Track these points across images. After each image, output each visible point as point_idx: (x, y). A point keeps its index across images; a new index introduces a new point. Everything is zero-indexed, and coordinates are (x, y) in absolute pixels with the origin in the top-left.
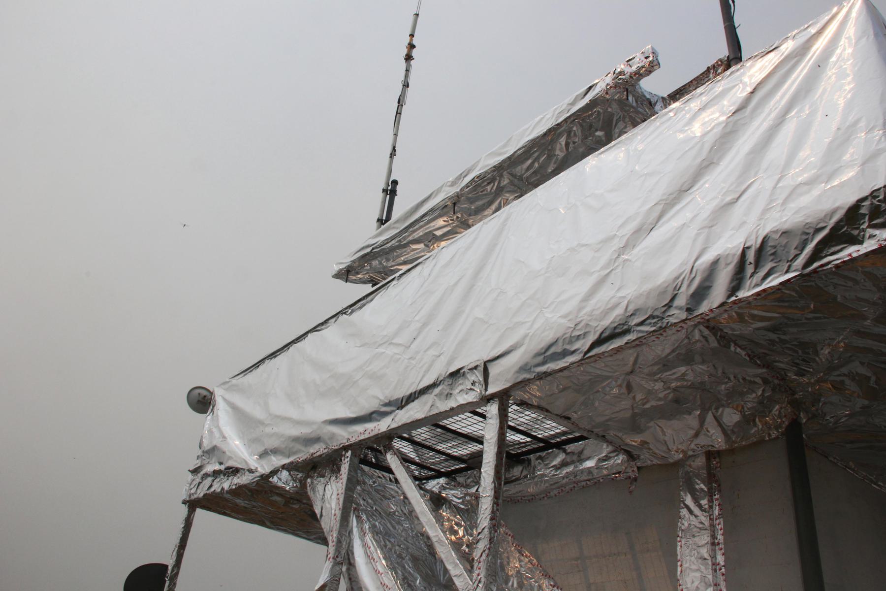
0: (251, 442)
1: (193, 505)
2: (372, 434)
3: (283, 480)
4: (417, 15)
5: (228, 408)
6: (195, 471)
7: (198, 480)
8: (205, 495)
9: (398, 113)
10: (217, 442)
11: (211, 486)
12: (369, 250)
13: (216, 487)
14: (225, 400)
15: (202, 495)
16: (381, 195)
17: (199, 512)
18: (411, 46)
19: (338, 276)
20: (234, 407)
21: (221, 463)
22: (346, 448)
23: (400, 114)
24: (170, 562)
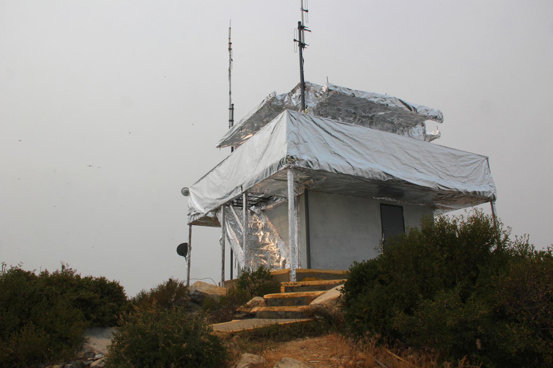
0: (202, 205)
1: (190, 224)
2: (226, 202)
3: (211, 215)
4: (230, 28)
5: (193, 195)
6: (189, 215)
7: (190, 217)
8: (193, 221)
9: (230, 76)
10: (193, 206)
11: (194, 219)
12: (223, 140)
13: (195, 219)
14: (193, 193)
15: (192, 222)
16: (228, 110)
17: (193, 226)
18: (230, 44)
19: (218, 147)
20: (195, 194)
21: (195, 212)
22: (221, 205)
23: (230, 76)
24: (188, 242)
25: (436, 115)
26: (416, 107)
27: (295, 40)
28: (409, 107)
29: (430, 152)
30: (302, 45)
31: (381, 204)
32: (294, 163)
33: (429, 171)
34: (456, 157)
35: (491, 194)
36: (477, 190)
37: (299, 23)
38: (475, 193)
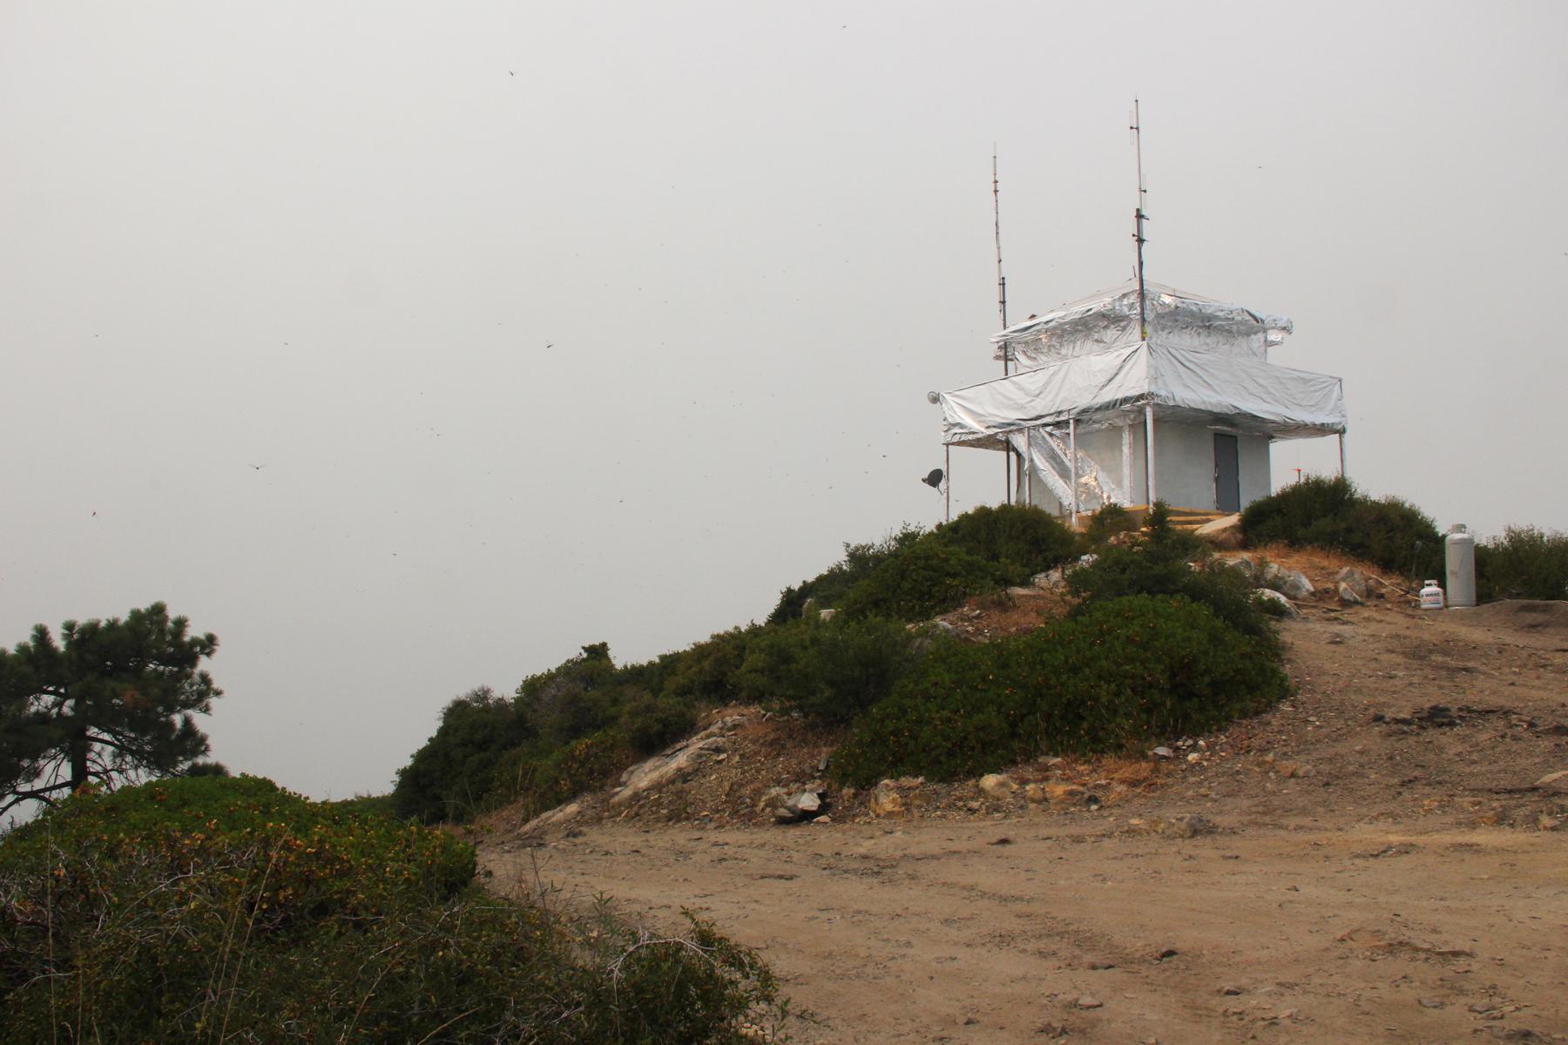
18: (996, 182)
25: (1285, 325)
26: (1264, 318)
27: (1134, 235)
28: (1256, 319)
29: (1278, 378)
30: (1140, 241)
31: (1216, 434)
32: (1153, 399)
33: (1274, 400)
34: (1305, 381)
35: (1341, 426)
36: (1325, 422)
37: (1138, 210)
38: (1323, 424)
